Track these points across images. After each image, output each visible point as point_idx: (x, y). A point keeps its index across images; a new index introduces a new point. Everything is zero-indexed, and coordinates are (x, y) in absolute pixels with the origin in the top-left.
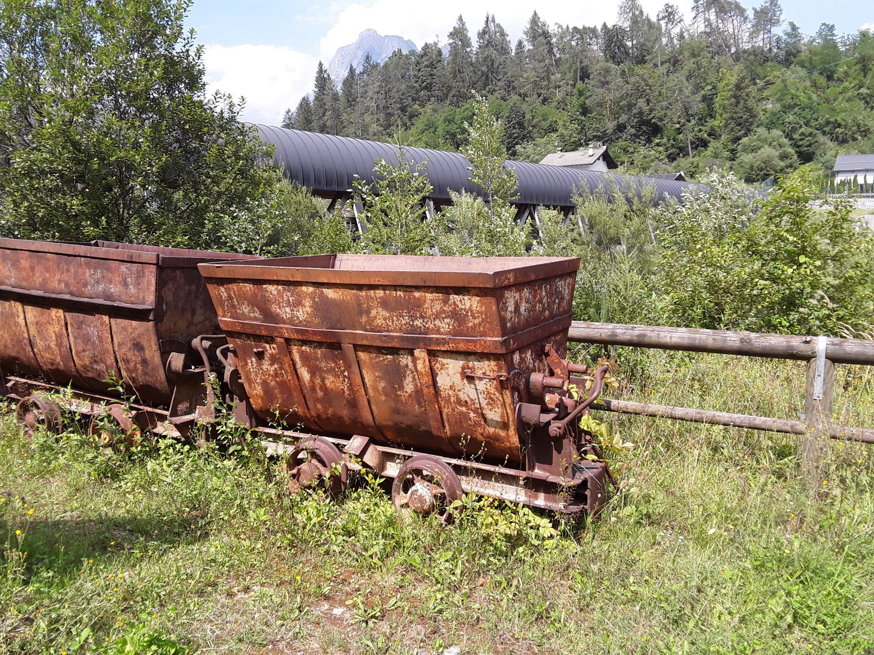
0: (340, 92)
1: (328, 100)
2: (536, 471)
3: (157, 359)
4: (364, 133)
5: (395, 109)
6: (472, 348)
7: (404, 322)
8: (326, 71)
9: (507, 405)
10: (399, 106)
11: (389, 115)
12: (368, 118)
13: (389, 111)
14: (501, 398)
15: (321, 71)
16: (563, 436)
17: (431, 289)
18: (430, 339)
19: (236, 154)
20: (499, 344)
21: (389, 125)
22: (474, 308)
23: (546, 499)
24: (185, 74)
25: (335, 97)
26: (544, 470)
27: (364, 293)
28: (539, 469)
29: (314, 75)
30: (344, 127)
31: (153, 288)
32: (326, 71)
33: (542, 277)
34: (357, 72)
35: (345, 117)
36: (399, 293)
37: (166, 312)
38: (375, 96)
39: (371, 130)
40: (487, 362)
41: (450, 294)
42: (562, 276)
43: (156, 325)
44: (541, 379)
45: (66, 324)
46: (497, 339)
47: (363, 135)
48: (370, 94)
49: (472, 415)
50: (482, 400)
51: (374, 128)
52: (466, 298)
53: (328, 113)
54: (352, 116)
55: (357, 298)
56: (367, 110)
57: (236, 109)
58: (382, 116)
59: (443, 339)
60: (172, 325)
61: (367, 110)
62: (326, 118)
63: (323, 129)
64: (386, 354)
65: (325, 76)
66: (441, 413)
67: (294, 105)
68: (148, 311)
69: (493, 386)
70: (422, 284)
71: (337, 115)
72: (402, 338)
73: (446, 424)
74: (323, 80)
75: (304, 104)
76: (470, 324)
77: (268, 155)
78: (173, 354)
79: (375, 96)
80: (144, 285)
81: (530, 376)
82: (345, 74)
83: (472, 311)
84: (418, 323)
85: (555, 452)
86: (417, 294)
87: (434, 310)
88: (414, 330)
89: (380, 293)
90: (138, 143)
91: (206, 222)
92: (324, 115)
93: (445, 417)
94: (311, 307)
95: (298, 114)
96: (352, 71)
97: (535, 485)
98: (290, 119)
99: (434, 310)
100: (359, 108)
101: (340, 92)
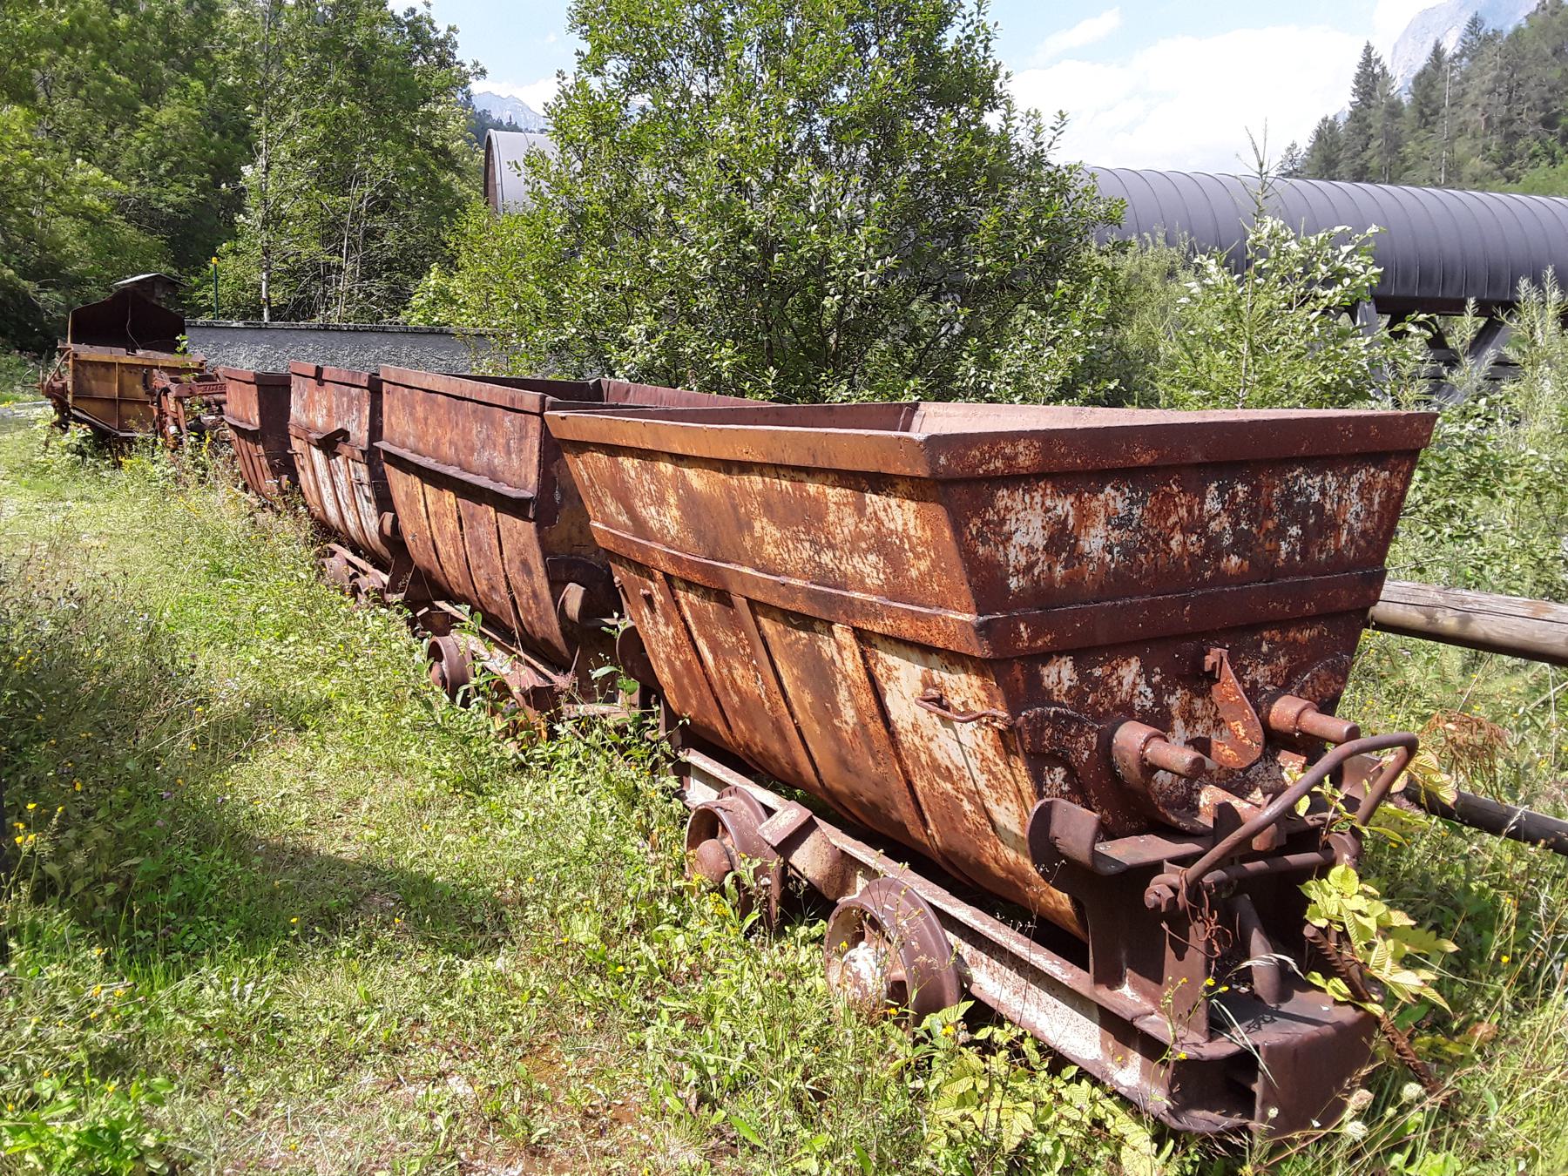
0: (1406, 99)
1: (1377, 120)
2: (1126, 990)
3: (546, 594)
4: (1454, 176)
5: (1529, 121)
6: (925, 636)
7: (805, 555)
8: (1378, 61)
9: (1025, 795)
10: (1539, 115)
11: (1513, 137)
12: (1462, 147)
13: (1514, 127)
14: (1009, 777)
15: (1368, 60)
16: (1179, 919)
17: (831, 478)
18: (851, 601)
19: (1033, 223)
20: (972, 632)
21: (1511, 158)
22: (912, 532)
23: (1144, 1072)
24: (969, 85)
25: (1394, 110)
26: (1144, 993)
27: (734, 481)
28: (1133, 985)
29: (1352, 69)
30: (1408, 169)
31: (535, 460)
32: (1378, 61)
33: (1198, 457)
34: (1449, 53)
35: (1410, 148)
36: (784, 483)
37: (562, 506)
38: (1484, 100)
39: (1467, 171)
40: (963, 676)
41: (863, 491)
42: (1377, 458)
43: (539, 529)
44: (1139, 743)
45: (460, 518)
46: (967, 617)
47: (1448, 181)
48: (1472, 97)
49: (967, 806)
50: (976, 773)
51: (1476, 164)
52: (893, 502)
53: (1374, 144)
54: (1429, 145)
55: (729, 488)
56: (1462, 131)
57: (1047, 136)
58: (1495, 141)
59: (872, 604)
60: (575, 531)
61: (1462, 131)
62: (1369, 153)
63: (1360, 175)
64: (798, 628)
65: (1377, 70)
66: (910, 785)
67: (1305, 141)
68: (527, 501)
69: (988, 740)
70: (809, 463)
71: (1394, 145)
72: (812, 596)
73: (928, 816)
74: (1370, 79)
75: (1326, 136)
76: (914, 573)
77: (1110, 220)
78: (572, 586)
79: (1484, 100)
80: (526, 454)
81: (1115, 730)
82: (1421, 60)
83: (909, 538)
84: (826, 558)
85: (1169, 953)
86: (812, 488)
87: (846, 531)
88: (823, 576)
89: (756, 482)
90: (845, 223)
91: (965, 355)
92: (1365, 147)
93: (921, 799)
94: (678, 508)
95: (1312, 151)
96: (1437, 52)
97: (1122, 1030)
98: (1292, 162)
99: (846, 531)
100: (1444, 127)
101: (1406, 99)
